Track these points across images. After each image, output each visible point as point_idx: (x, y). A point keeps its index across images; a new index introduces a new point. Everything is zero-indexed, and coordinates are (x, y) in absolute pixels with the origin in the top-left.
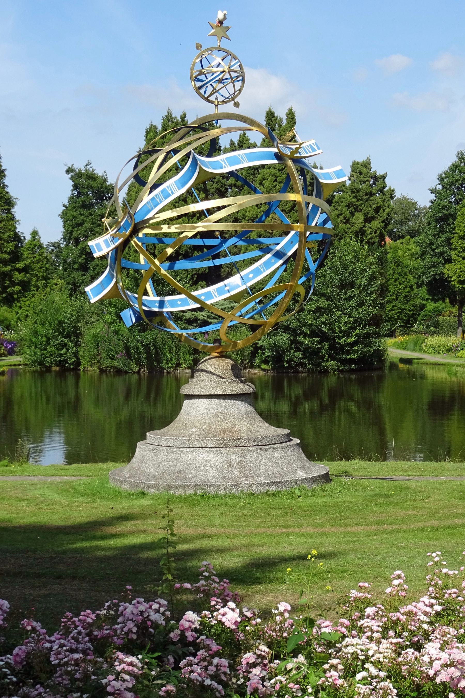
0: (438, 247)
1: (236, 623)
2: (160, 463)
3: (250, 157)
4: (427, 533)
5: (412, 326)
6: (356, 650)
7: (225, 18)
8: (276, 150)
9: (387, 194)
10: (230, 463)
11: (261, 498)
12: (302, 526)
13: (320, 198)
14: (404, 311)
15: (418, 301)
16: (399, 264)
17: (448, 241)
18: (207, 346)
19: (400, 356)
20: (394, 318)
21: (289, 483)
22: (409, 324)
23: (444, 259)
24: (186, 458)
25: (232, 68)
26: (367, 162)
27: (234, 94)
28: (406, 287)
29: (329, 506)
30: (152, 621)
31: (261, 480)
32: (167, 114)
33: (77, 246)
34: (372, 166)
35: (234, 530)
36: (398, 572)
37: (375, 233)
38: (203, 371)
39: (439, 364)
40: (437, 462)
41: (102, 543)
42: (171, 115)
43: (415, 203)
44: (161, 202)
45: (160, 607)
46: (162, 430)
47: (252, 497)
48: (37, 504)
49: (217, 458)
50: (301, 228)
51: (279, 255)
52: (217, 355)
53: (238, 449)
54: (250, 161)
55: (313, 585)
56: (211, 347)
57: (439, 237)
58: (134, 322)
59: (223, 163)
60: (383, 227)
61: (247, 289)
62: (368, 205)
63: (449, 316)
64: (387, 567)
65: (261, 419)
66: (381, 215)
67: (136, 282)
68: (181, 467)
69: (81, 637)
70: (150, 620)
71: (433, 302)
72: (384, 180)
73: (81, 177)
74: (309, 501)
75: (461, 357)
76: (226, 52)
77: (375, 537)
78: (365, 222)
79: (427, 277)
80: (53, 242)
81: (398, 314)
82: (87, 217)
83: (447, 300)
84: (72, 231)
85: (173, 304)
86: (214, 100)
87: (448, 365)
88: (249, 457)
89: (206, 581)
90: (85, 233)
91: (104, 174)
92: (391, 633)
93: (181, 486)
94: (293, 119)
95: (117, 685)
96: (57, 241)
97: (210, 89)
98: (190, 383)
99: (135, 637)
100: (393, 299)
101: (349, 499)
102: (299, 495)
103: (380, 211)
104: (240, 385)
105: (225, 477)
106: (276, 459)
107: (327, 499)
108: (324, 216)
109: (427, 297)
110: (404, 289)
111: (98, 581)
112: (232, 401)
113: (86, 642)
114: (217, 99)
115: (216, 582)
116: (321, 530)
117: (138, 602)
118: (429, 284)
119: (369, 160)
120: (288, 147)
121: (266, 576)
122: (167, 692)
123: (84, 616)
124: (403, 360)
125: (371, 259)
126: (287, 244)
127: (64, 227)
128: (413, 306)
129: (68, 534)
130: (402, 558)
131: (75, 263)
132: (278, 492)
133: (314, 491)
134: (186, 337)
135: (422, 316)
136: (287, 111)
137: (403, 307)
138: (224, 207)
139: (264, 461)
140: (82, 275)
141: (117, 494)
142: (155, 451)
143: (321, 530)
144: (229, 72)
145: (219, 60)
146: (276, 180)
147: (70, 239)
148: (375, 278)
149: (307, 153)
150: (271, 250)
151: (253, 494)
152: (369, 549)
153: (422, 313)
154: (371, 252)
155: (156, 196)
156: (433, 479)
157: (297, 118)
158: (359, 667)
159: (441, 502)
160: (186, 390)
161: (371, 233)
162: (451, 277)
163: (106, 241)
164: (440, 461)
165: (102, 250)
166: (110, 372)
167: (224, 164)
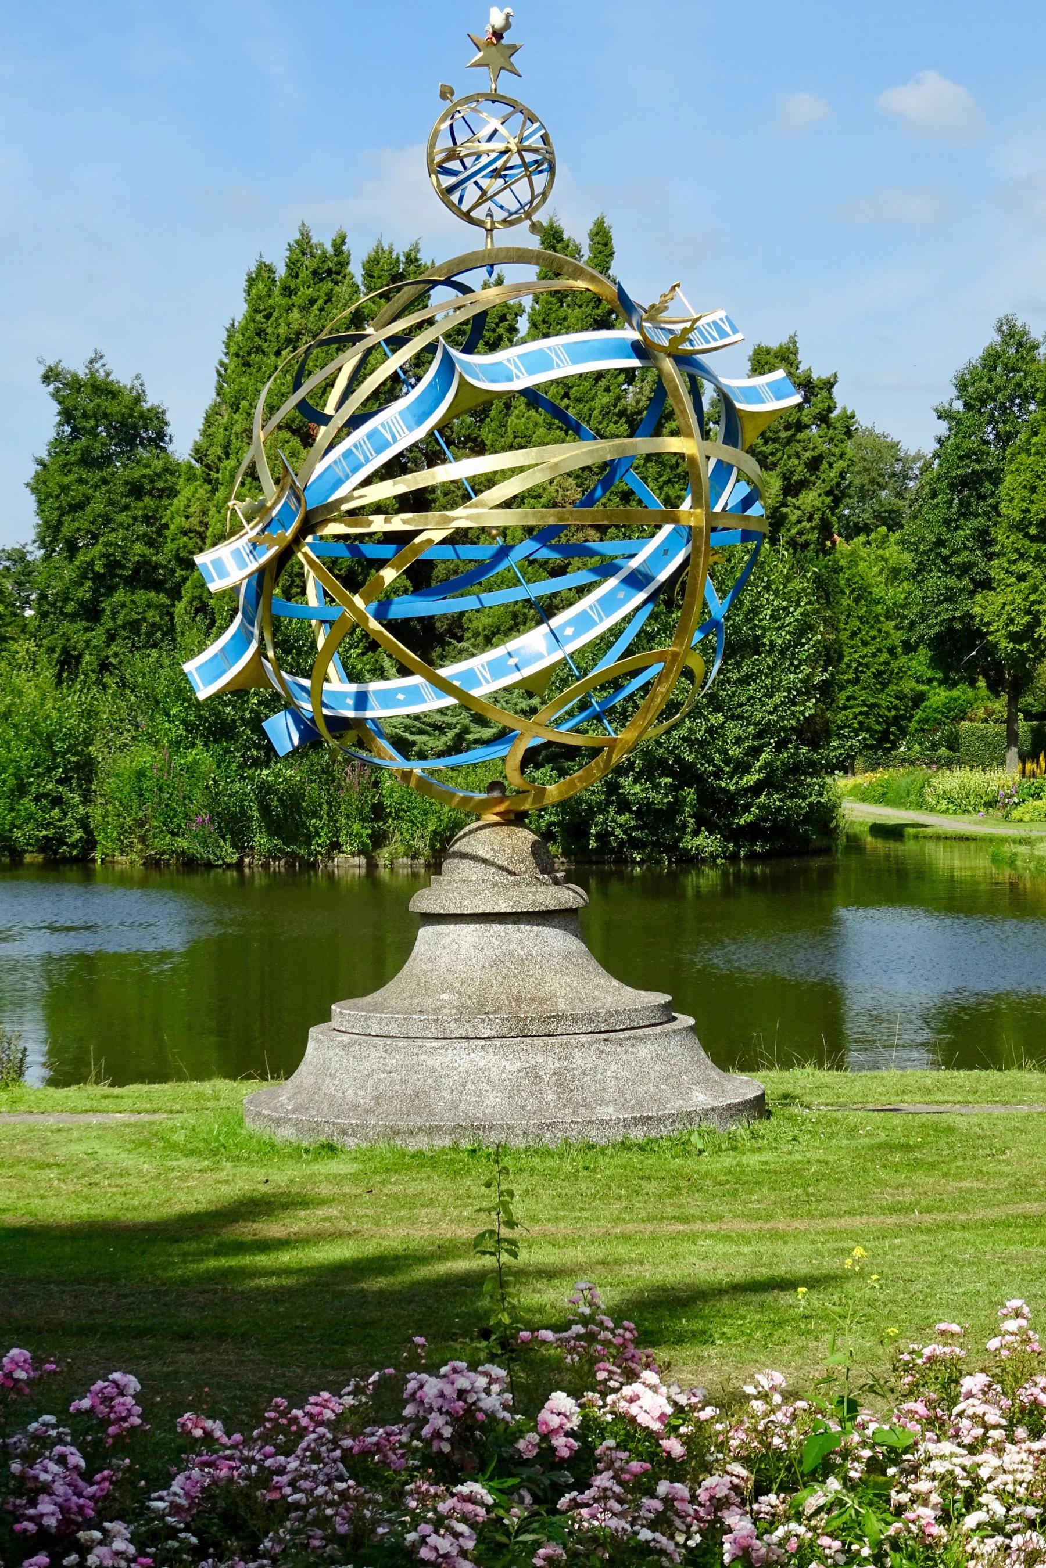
0: (955, 552)
1: (662, 1417)
2: (368, 1075)
3: (576, 354)
4: (1018, 1230)
5: (895, 747)
6: (951, 1467)
7: (507, 26)
8: (636, 336)
9: (838, 425)
10: (534, 1075)
11: (612, 1157)
12: (721, 1218)
13: (736, 446)
14: (876, 710)
15: (908, 686)
16: (862, 594)
17: (984, 539)
18: (472, 798)
19: (871, 820)
20: (849, 726)
21: (674, 1118)
22: (888, 741)
23: (972, 580)
24: (430, 1063)
25: (526, 144)
26: (788, 349)
27: (531, 202)
28: (880, 650)
29: (776, 1172)
30: (485, 1412)
31: (608, 1112)
32: (298, 236)
33: (71, 558)
34: (800, 357)
35: (564, 1228)
36: (1016, 1303)
37: (810, 519)
38: (464, 856)
39: (967, 839)
40: (1000, 1070)
41: (263, 1260)
42: (309, 239)
43: (894, 446)
44: (367, 461)
45: (490, 1383)
46: (369, 999)
47: (591, 1154)
48: (84, 1176)
49: (504, 1063)
50: (696, 517)
51: (636, 580)
52: (496, 819)
53: (553, 1040)
54: (575, 361)
55: (778, 1348)
56: (482, 801)
57: (957, 528)
58: (296, 742)
59: (512, 367)
60: (828, 507)
61: (565, 659)
62: (792, 452)
63: (986, 721)
64: (941, 1305)
65: (602, 970)
66: (823, 476)
67: (295, 650)
68: (419, 1084)
69: (324, 1448)
70: (480, 1410)
71: (943, 687)
72: (830, 392)
73: (78, 391)
74: (727, 1160)
75: (1021, 821)
76: (512, 104)
77: (897, 1241)
78: (785, 495)
79: (929, 627)
80: (8, 548)
81: (860, 718)
82: (96, 487)
83: (982, 683)
84: (60, 522)
85: (388, 699)
86: (483, 218)
87: (991, 840)
88: (580, 1059)
89: (585, 1324)
90: (93, 528)
91: (137, 383)
92: (1021, 1432)
93: (420, 1129)
94: (606, 245)
95: (444, 1544)
96: (18, 547)
97: (472, 194)
98: (434, 885)
99: (446, 1448)
100: (849, 681)
101: (820, 1155)
102: (700, 1146)
103: (822, 468)
104: (554, 889)
105: (523, 1108)
106: (641, 1062)
107: (767, 1156)
108: (744, 490)
109: (930, 674)
110: (874, 655)
111: (279, 1343)
112: (535, 928)
113: (335, 1462)
114: (492, 216)
115: (607, 1329)
116: (769, 1226)
117: (455, 1371)
118: (937, 642)
119: (795, 343)
120: (662, 329)
121: (667, 1328)
122: (548, 1558)
123: (316, 1404)
124: (880, 830)
125: (796, 585)
126: (657, 553)
127: (41, 511)
128: (897, 698)
129: (177, 1241)
130: (971, 1286)
131: (67, 600)
132: (650, 1141)
133: (732, 1138)
134: (420, 779)
135: (919, 722)
136: (591, 226)
137: (872, 700)
138: (521, 469)
139: (613, 1067)
140: (87, 630)
141: (270, 1150)
142: (357, 1047)
143: (769, 1226)
144: (519, 152)
145: (495, 123)
146: (566, 395)
147: (55, 540)
148: (811, 628)
149: (708, 342)
150: (618, 569)
151: (591, 1147)
152: (892, 1265)
153: (918, 714)
154: (799, 566)
155: (355, 446)
156: (999, 1111)
157: (615, 243)
158: (957, 1505)
159: (1035, 1160)
160: (424, 902)
161: (799, 522)
162: (989, 624)
163: (237, 553)
164: (1008, 1068)
165: (227, 575)
166: (167, 864)
167: (515, 371)
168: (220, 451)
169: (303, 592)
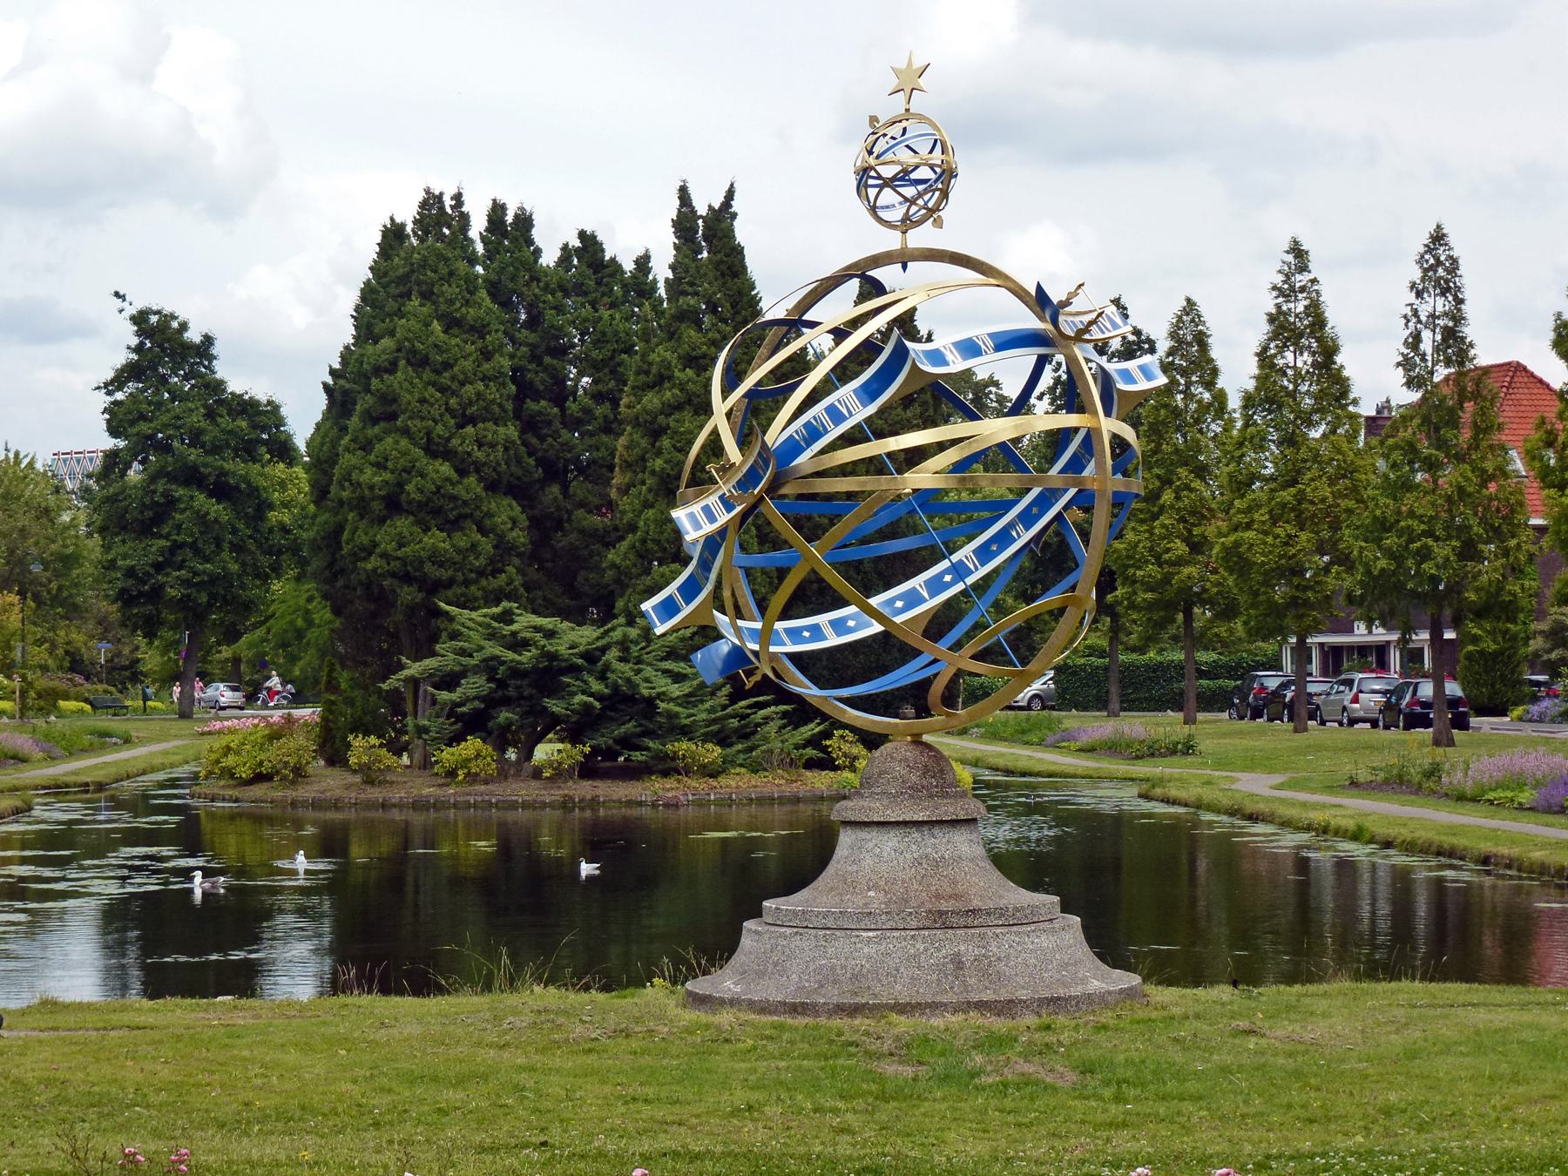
168: (213, 547)
169: (535, 612)
